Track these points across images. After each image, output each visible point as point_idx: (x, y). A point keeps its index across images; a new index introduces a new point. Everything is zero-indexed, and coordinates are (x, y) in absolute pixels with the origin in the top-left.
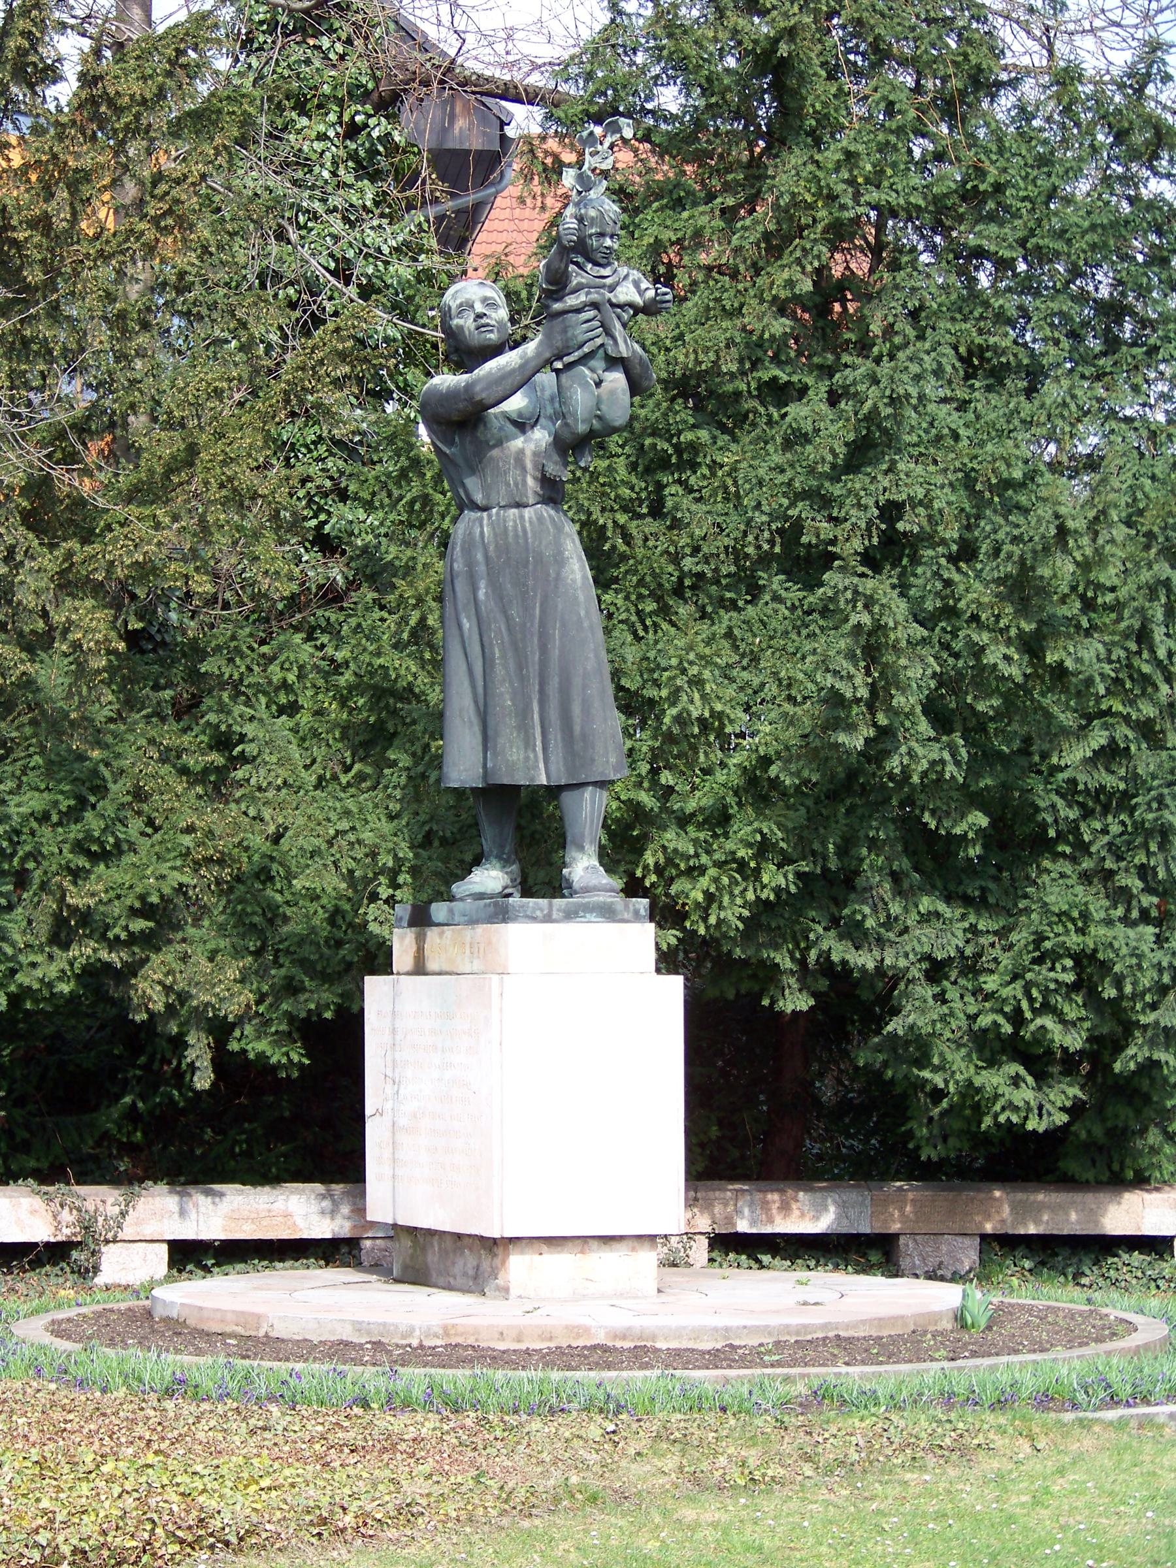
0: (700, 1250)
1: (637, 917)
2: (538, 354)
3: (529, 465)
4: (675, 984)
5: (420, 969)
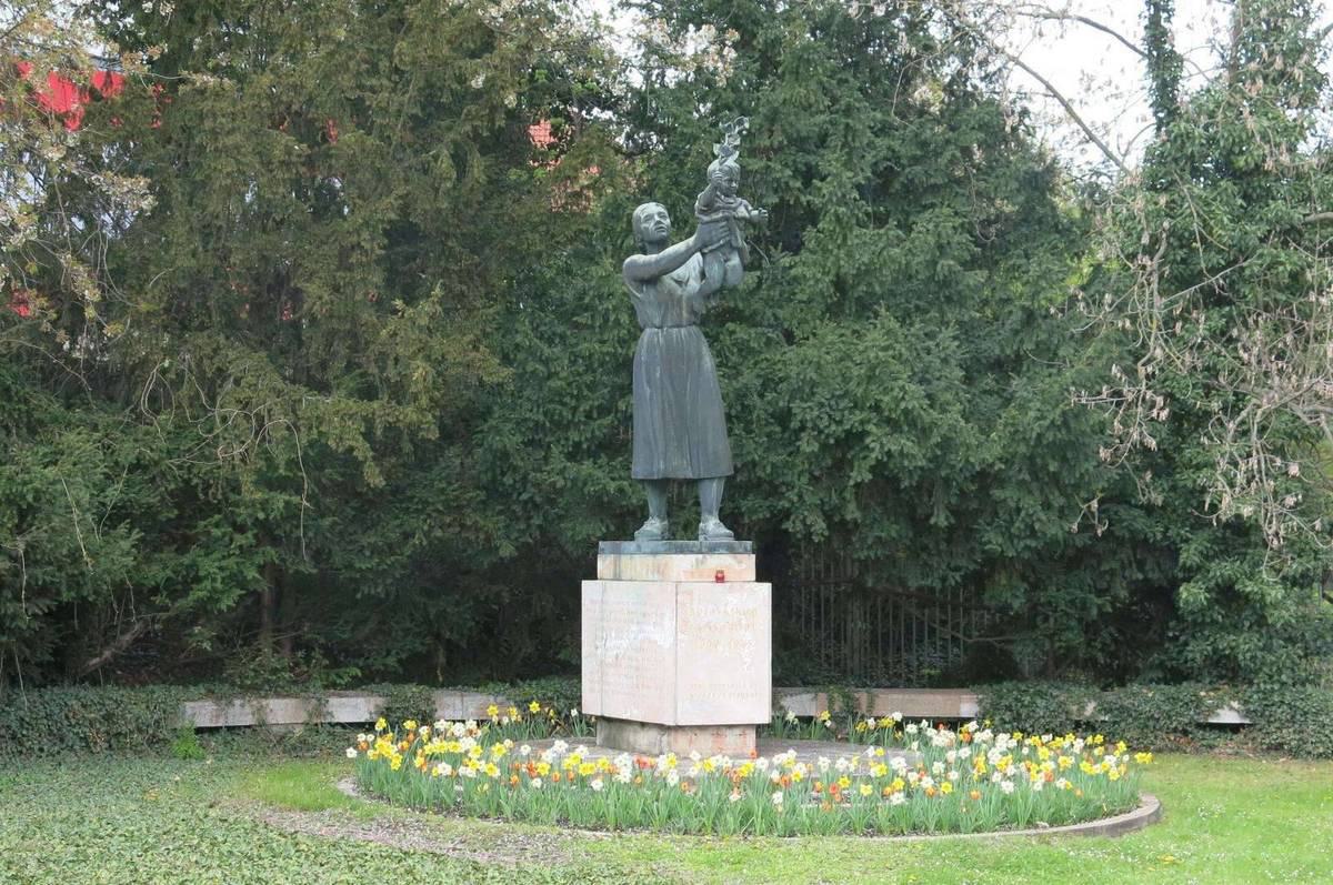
0: (1265, 423)
1: (746, 551)
2: (695, 245)
3: (684, 305)
4: (767, 588)
5: (617, 578)
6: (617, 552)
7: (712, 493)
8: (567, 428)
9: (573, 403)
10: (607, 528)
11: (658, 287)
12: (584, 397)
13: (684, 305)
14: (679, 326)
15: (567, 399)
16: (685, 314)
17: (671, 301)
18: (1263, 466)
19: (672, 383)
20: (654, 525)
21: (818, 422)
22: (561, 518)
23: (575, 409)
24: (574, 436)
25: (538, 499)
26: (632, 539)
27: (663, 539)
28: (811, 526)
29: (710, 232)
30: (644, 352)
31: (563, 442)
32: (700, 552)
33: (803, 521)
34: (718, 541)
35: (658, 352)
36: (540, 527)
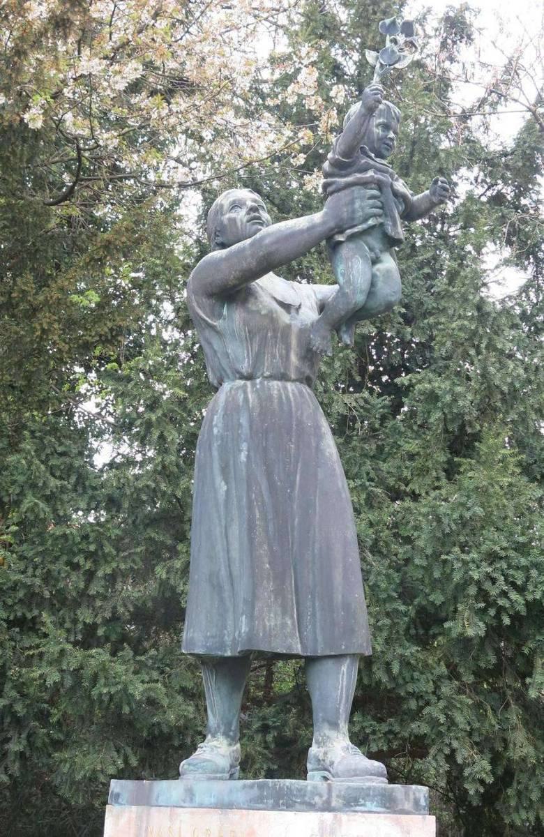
1: (417, 807)
3: (294, 342)
6: (143, 800)
7: (336, 687)
8: (77, 604)
9: (88, 565)
10: (126, 761)
11: (251, 306)
12: (105, 556)
13: (294, 342)
14: (284, 377)
15: (79, 559)
16: (294, 358)
17: (267, 332)
18: (218, 775)
19: (269, 475)
20: (217, 750)
21: (487, 586)
22: (58, 745)
23: (90, 576)
24: (85, 615)
25: (19, 708)
26: (177, 776)
27: (231, 777)
28: (465, 765)
29: (352, 202)
30: (217, 419)
31: (68, 625)
32: (327, 807)
33: (451, 758)
34: (357, 783)
35: (244, 421)
36: (21, 755)
